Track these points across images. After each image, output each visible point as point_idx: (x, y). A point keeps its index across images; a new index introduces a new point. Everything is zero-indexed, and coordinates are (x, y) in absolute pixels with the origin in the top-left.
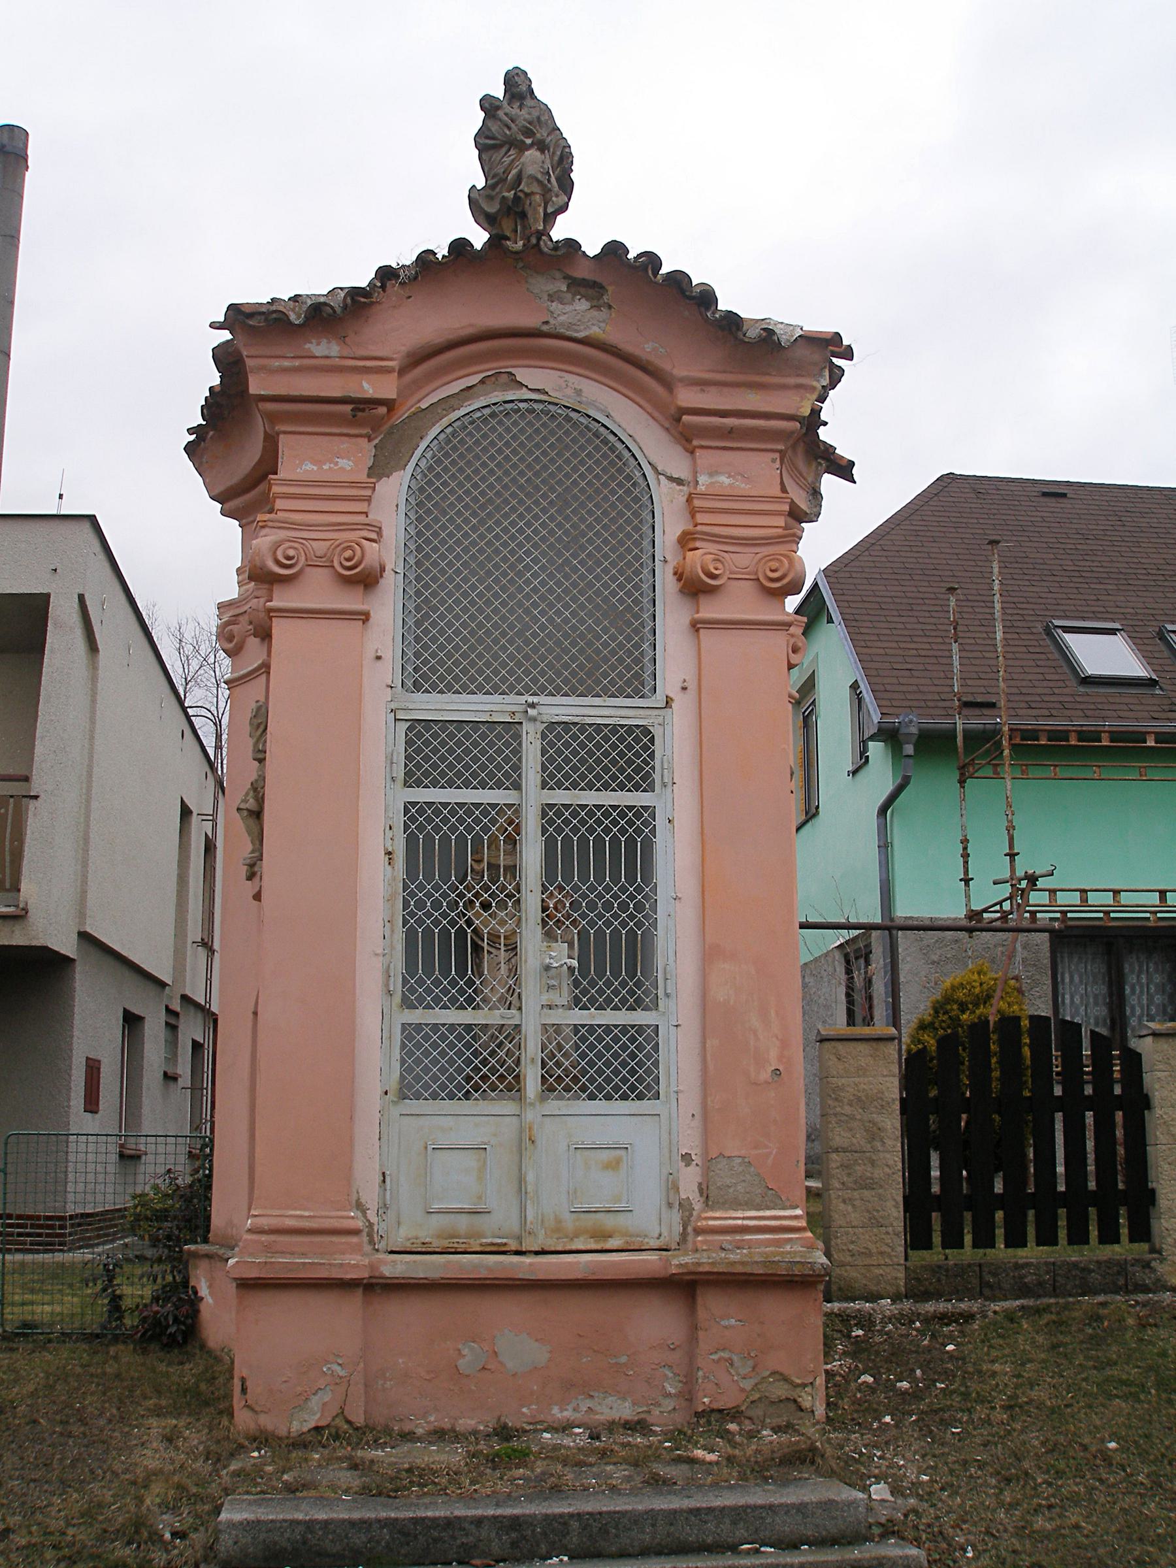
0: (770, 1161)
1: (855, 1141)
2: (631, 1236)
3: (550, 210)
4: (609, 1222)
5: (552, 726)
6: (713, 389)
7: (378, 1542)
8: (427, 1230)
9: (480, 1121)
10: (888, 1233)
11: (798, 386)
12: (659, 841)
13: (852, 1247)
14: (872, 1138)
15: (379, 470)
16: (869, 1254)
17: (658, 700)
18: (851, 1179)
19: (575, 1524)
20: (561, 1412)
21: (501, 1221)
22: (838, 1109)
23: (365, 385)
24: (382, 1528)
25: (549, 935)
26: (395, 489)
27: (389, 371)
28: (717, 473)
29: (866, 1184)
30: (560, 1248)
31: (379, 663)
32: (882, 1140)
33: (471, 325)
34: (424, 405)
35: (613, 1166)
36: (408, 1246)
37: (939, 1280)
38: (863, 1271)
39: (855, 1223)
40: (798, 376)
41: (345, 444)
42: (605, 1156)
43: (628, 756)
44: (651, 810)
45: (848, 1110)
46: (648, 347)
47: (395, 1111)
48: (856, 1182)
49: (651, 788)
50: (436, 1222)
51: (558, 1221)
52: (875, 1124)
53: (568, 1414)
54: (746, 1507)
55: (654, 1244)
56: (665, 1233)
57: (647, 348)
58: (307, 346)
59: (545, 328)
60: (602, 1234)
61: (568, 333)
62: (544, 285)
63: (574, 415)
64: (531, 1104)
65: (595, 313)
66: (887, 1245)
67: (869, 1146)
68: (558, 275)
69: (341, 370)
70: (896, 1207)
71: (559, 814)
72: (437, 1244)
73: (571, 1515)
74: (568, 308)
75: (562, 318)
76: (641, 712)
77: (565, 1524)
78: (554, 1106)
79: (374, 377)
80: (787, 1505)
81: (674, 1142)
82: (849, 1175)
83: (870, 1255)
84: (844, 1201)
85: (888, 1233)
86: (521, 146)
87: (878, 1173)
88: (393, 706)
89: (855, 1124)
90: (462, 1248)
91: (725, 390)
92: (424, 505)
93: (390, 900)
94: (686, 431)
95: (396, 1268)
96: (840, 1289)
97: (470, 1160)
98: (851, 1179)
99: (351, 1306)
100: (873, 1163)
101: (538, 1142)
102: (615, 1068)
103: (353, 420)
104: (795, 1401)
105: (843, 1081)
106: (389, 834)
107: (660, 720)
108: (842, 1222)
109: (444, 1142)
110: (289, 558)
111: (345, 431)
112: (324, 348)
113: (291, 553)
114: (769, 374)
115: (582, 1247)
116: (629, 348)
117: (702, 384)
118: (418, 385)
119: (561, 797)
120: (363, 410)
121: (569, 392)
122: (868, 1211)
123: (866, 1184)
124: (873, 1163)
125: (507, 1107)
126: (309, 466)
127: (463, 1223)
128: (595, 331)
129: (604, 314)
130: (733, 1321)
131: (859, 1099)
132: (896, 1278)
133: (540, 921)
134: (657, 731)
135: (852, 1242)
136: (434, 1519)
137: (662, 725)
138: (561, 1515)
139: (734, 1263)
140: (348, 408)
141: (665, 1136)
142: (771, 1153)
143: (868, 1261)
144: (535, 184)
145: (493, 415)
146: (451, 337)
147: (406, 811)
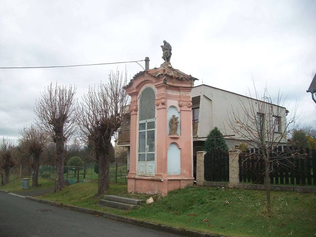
9: (142, 163)
17: (155, 118)
21: (144, 174)
27: (135, 89)
43: (152, 125)
60: (150, 175)
72: (141, 175)
78: (147, 162)
95: (137, 177)
97: (142, 167)
102: (151, 158)
103: (135, 94)
125: (144, 162)
127: (142, 173)
134: (155, 122)
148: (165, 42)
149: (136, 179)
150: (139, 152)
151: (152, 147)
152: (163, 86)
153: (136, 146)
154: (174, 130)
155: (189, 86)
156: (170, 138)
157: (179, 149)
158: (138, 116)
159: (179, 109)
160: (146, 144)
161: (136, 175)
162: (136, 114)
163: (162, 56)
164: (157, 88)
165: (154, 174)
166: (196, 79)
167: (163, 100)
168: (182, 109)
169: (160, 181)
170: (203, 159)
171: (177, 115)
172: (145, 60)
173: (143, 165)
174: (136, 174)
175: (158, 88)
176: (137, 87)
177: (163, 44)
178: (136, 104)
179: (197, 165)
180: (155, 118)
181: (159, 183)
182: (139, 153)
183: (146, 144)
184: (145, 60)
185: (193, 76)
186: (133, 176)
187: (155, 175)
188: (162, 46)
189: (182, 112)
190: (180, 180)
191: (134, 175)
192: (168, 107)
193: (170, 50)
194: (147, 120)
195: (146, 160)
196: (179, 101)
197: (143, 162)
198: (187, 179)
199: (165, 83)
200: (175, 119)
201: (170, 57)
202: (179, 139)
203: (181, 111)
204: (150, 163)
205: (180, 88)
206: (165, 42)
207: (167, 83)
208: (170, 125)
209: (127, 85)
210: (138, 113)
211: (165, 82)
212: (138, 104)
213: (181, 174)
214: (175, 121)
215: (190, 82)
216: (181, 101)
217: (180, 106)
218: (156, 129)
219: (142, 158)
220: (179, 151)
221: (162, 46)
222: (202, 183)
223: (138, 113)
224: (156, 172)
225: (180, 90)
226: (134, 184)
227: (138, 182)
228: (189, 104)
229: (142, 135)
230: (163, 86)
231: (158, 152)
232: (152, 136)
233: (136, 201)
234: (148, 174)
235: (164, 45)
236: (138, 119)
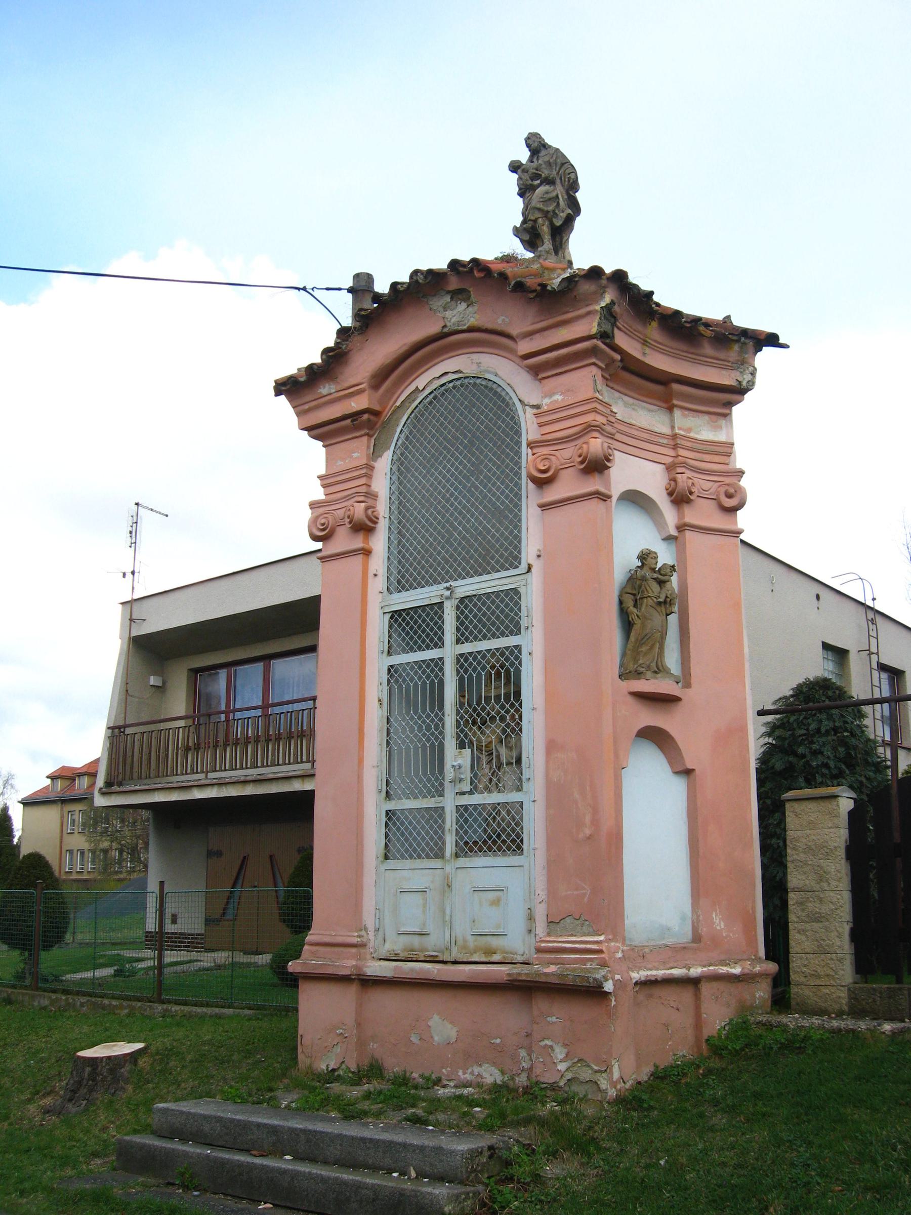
0: (586, 900)
1: (807, 882)
2: (507, 953)
3: (558, 223)
4: (495, 942)
5: (462, 600)
6: (538, 335)
7: (215, 1131)
8: (395, 944)
9: (417, 874)
10: (832, 959)
11: (589, 313)
12: (523, 669)
13: (804, 969)
14: (821, 879)
15: (376, 453)
16: (819, 977)
17: (523, 567)
18: (804, 914)
19: (303, 1137)
20: (464, 1074)
21: (435, 942)
22: (795, 857)
23: (353, 404)
24: (217, 1122)
25: (461, 746)
26: (384, 464)
27: (361, 391)
28: (554, 394)
29: (817, 918)
30: (465, 960)
31: (377, 578)
32: (827, 881)
33: (405, 344)
34: (398, 404)
35: (496, 903)
36: (388, 956)
37: (874, 1001)
38: (815, 990)
39: (807, 950)
40: (587, 306)
41: (355, 444)
42: (492, 895)
43: (502, 613)
44: (518, 647)
45: (802, 856)
46: (500, 321)
47: (383, 868)
48: (808, 916)
49: (518, 633)
50: (404, 941)
51: (465, 941)
52: (822, 868)
53: (468, 1077)
54: (391, 1142)
55: (520, 959)
56: (527, 952)
57: (500, 321)
58: (320, 390)
59: (446, 330)
60: (490, 952)
61: (460, 328)
62: (439, 302)
63: (478, 381)
64: (448, 861)
65: (470, 309)
66: (831, 968)
67: (818, 886)
68: (443, 293)
69: (339, 399)
70: (840, 936)
71: (466, 660)
72: (402, 955)
73: (301, 1130)
74: (455, 312)
75: (453, 320)
76: (513, 579)
77: (298, 1135)
78: (462, 862)
79: (357, 398)
80: (415, 1146)
81: (532, 885)
82: (803, 910)
83: (819, 977)
84: (799, 932)
85: (832, 959)
86: (548, 187)
87: (825, 909)
88: (383, 604)
89: (807, 869)
90: (415, 957)
91: (546, 333)
92: (401, 467)
93: (380, 731)
94: (541, 368)
95: (376, 968)
96: (797, 1004)
97: (417, 898)
98: (804, 914)
99: (352, 991)
100: (821, 900)
101: (453, 886)
102: (497, 835)
103: (356, 428)
104: (596, 1083)
105: (799, 833)
106: (380, 688)
107: (524, 582)
108: (798, 949)
109: (406, 887)
110: (323, 524)
111: (354, 435)
112: (326, 389)
113: (323, 521)
114: (568, 312)
115: (477, 960)
116: (490, 326)
117: (530, 334)
118: (391, 392)
119: (467, 648)
120: (356, 420)
121: (474, 367)
122: (817, 940)
123: (817, 918)
124: (821, 900)
125: (437, 863)
126: (340, 463)
127: (416, 941)
128: (473, 321)
129: (476, 308)
130: (554, 1019)
131: (810, 848)
132: (840, 997)
133: (454, 735)
134: (522, 590)
135: (805, 966)
136: (239, 1121)
137: (526, 585)
138: (296, 1129)
139: (546, 974)
140: (348, 421)
141: (527, 880)
142: (585, 894)
143: (818, 982)
144: (536, 212)
145: (435, 398)
146: (395, 356)
147: (389, 671)
148: (536, 145)
149: (368, 983)
150: (388, 796)
151: (499, 758)
152: (594, 351)
153: (361, 761)
154: (652, 647)
155: (726, 378)
156: (630, 699)
157: (677, 773)
158: (379, 562)
159: (670, 516)
160: (450, 744)
161: (362, 950)
162: (367, 552)
163: (518, 220)
164: (536, 371)
165: (517, 942)
166: (772, 340)
167: (596, 445)
168: (691, 516)
169: (593, 992)
170: (838, 836)
171: (665, 556)
172: (350, 290)
173: (421, 886)
174: (363, 945)
175: (574, 361)
176: (381, 377)
177: (524, 156)
178: (363, 489)
179: (794, 879)
180: (523, 567)
181: (582, 1012)
182: (391, 805)
183: (450, 744)
184: (350, 290)
185: (739, 322)
186: (346, 964)
187: (539, 950)
188: (515, 167)
189: (688, 534)
190: (694, 982)
191: (354, 950)
192: (616, 493)
193: (573, 186)
194: (460, 582)
195: (448, 853)
196: (670, 468)
197: (427, 863)
198: (737, 970)
199: (605, 336)
200: (655, 575)
201: (569, 222)
202: (679, 711)
203: (681, 528)
204: (487, 869)
205: (676, 386)
206: (536, 145)
207: (621, 340)
208: (624, 612)
209: (311, 368)
210: (380, 543)
211: (607, 327)
212: (381, 484)
213: (697, 938)
214: (655, 587)
215: (733, 353)
216: (684, 465)
217: (680, 498)
218: (532, 644)
219: (407, 838)
220: (678, 787)
221: (515, 167)
222: (843, 994)
223: (380, 543)
224: (541, 929)
225: (675, 402)
226: (350, 1020)
227: (387, 1004)
228: (732, 491)
229: (414, 692)
230: (594, 351)
231: (556, 794)
232: (494, 693)
233: (452, 1152)
234: (471, 942)
235: (531, 160)
236: (377, 584)
